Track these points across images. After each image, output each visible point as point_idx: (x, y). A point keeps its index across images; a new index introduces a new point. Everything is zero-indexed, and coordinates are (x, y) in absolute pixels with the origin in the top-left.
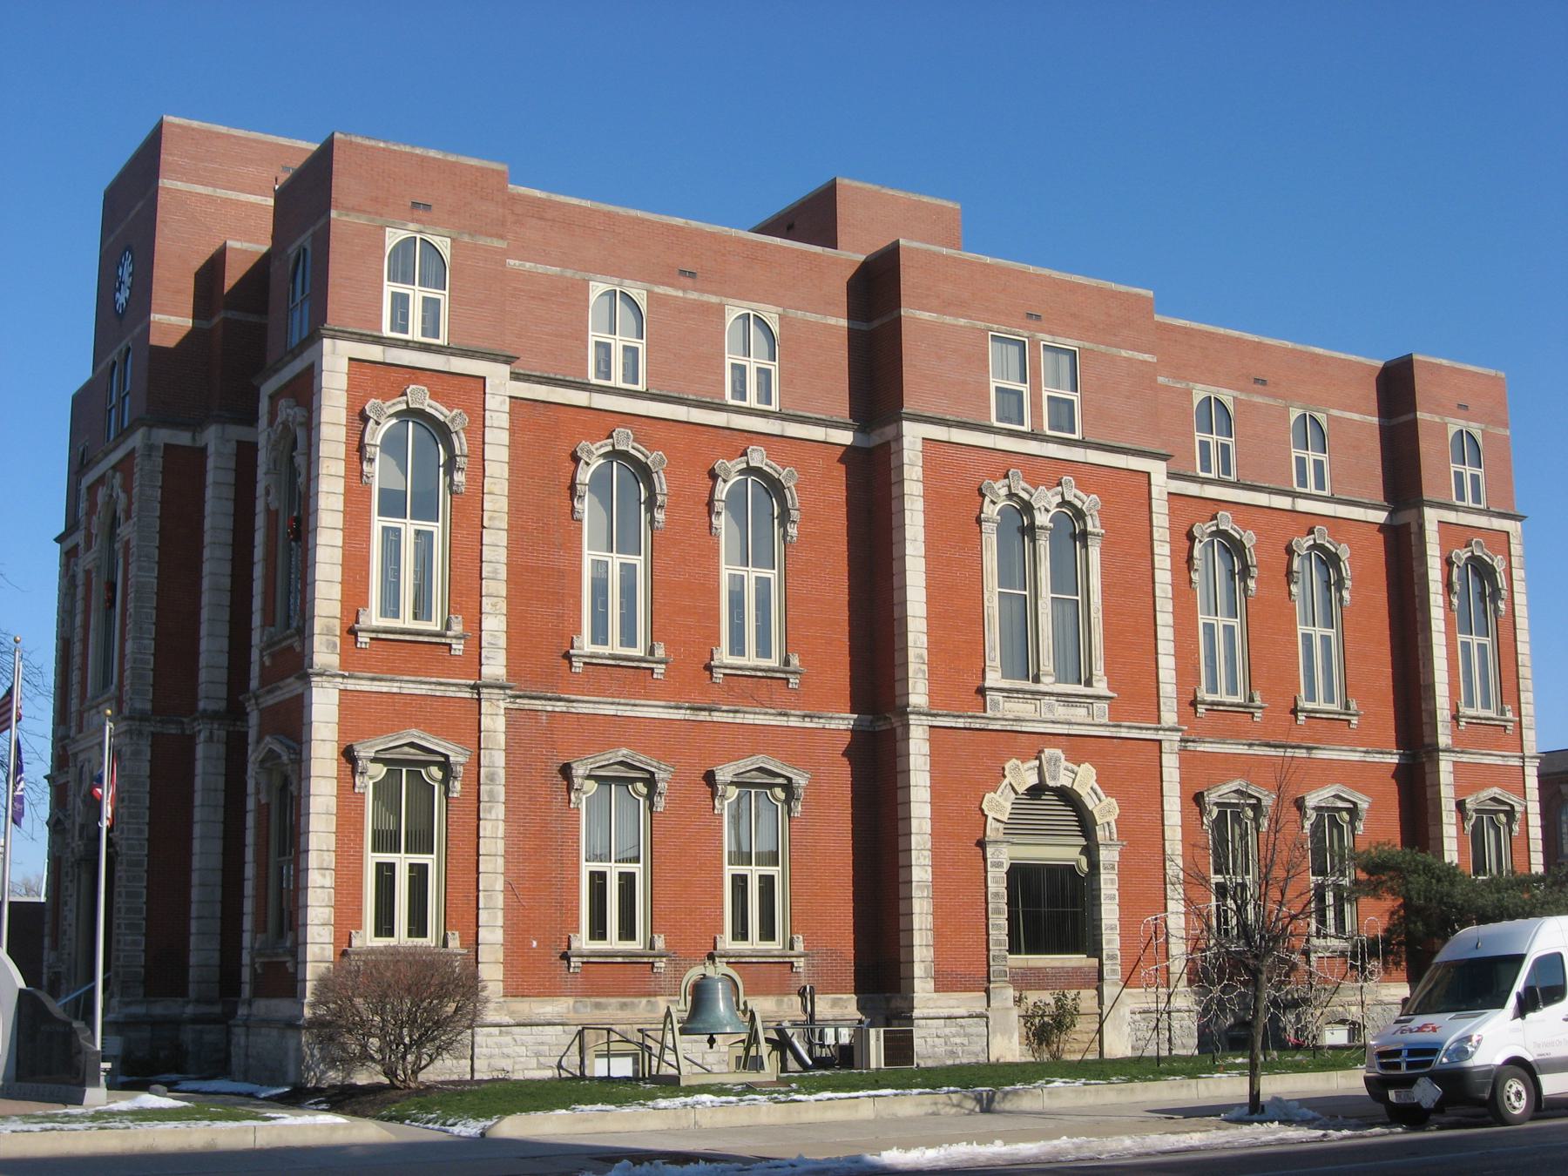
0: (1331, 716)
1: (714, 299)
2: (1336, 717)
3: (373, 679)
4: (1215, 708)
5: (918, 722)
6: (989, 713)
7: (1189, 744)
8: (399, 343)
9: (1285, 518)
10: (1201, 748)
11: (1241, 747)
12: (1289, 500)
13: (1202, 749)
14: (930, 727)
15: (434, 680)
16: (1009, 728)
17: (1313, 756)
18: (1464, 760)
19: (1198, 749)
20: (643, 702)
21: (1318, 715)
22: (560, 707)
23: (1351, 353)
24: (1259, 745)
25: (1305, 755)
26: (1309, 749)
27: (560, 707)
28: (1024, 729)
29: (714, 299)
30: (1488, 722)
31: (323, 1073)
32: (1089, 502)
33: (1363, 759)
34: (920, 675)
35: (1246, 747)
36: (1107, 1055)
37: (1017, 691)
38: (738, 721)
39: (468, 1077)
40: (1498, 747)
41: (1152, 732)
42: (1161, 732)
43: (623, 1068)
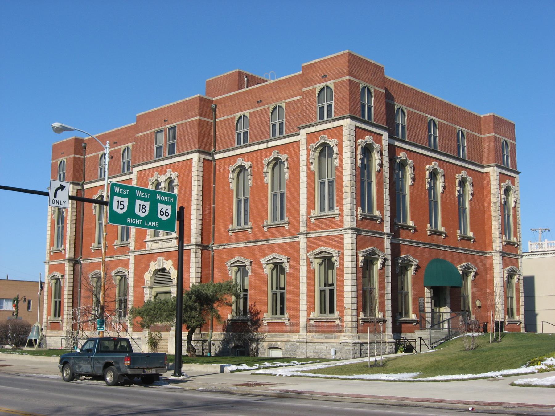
0: (277, 226)
1: (311, 88)
2: (279, 226)
3: (52, 262)
4: (235, 231)
5: (303, 237)
6: (147, 248)
7: (225, 246)
8: (274, 130)
9: (266, 151)
10: (230, 247)
11: (243, 244)
12: (266, 144)
13: (230, 247)
14: (135, 255)
15: (319, 231)
16: (151, 252)
17: (269, 243)
18: (313, 236)
19: (229, 247)
20: (120, 255)
21: (271, 227)
22: (89, 261)
23: (177, 101)
24: (248, 242)
25: (266, 243)
26: (267, 240)
27: (89, 261)
28: (154, 252)
29: (311, 88)
30: (325, 217)
31: (16, 340)
32: (174, 175)
33: (290, 241)
34: (133, 241)
35: (244, 244)
36: (108, 342)
37: (154, 241)
38: (119, 259)
39: (110, 342)
40: (332, 227)
41: (187, 247)
42: (189, 246)
43: (199, 341)
